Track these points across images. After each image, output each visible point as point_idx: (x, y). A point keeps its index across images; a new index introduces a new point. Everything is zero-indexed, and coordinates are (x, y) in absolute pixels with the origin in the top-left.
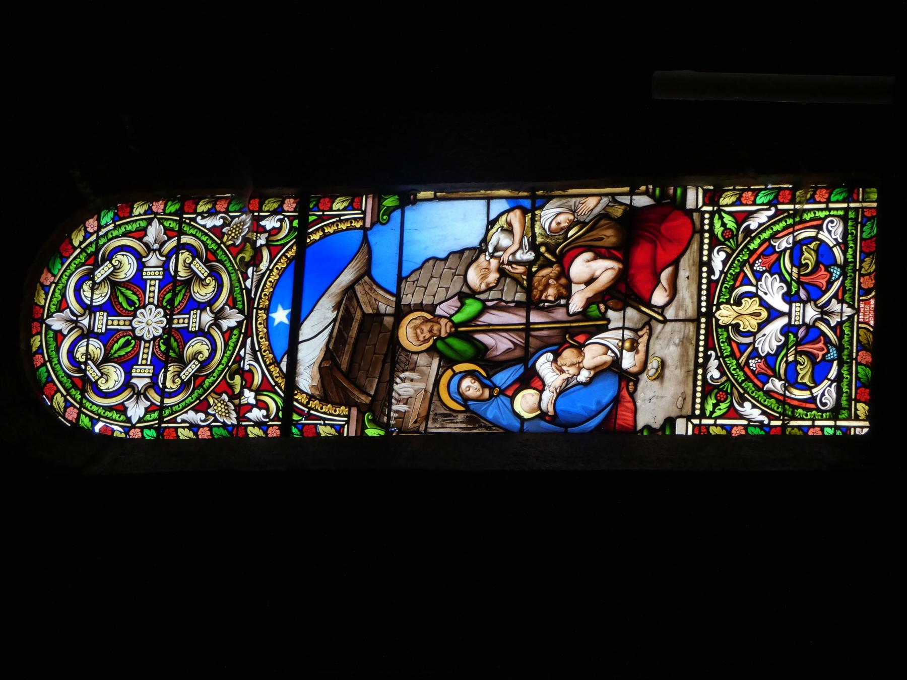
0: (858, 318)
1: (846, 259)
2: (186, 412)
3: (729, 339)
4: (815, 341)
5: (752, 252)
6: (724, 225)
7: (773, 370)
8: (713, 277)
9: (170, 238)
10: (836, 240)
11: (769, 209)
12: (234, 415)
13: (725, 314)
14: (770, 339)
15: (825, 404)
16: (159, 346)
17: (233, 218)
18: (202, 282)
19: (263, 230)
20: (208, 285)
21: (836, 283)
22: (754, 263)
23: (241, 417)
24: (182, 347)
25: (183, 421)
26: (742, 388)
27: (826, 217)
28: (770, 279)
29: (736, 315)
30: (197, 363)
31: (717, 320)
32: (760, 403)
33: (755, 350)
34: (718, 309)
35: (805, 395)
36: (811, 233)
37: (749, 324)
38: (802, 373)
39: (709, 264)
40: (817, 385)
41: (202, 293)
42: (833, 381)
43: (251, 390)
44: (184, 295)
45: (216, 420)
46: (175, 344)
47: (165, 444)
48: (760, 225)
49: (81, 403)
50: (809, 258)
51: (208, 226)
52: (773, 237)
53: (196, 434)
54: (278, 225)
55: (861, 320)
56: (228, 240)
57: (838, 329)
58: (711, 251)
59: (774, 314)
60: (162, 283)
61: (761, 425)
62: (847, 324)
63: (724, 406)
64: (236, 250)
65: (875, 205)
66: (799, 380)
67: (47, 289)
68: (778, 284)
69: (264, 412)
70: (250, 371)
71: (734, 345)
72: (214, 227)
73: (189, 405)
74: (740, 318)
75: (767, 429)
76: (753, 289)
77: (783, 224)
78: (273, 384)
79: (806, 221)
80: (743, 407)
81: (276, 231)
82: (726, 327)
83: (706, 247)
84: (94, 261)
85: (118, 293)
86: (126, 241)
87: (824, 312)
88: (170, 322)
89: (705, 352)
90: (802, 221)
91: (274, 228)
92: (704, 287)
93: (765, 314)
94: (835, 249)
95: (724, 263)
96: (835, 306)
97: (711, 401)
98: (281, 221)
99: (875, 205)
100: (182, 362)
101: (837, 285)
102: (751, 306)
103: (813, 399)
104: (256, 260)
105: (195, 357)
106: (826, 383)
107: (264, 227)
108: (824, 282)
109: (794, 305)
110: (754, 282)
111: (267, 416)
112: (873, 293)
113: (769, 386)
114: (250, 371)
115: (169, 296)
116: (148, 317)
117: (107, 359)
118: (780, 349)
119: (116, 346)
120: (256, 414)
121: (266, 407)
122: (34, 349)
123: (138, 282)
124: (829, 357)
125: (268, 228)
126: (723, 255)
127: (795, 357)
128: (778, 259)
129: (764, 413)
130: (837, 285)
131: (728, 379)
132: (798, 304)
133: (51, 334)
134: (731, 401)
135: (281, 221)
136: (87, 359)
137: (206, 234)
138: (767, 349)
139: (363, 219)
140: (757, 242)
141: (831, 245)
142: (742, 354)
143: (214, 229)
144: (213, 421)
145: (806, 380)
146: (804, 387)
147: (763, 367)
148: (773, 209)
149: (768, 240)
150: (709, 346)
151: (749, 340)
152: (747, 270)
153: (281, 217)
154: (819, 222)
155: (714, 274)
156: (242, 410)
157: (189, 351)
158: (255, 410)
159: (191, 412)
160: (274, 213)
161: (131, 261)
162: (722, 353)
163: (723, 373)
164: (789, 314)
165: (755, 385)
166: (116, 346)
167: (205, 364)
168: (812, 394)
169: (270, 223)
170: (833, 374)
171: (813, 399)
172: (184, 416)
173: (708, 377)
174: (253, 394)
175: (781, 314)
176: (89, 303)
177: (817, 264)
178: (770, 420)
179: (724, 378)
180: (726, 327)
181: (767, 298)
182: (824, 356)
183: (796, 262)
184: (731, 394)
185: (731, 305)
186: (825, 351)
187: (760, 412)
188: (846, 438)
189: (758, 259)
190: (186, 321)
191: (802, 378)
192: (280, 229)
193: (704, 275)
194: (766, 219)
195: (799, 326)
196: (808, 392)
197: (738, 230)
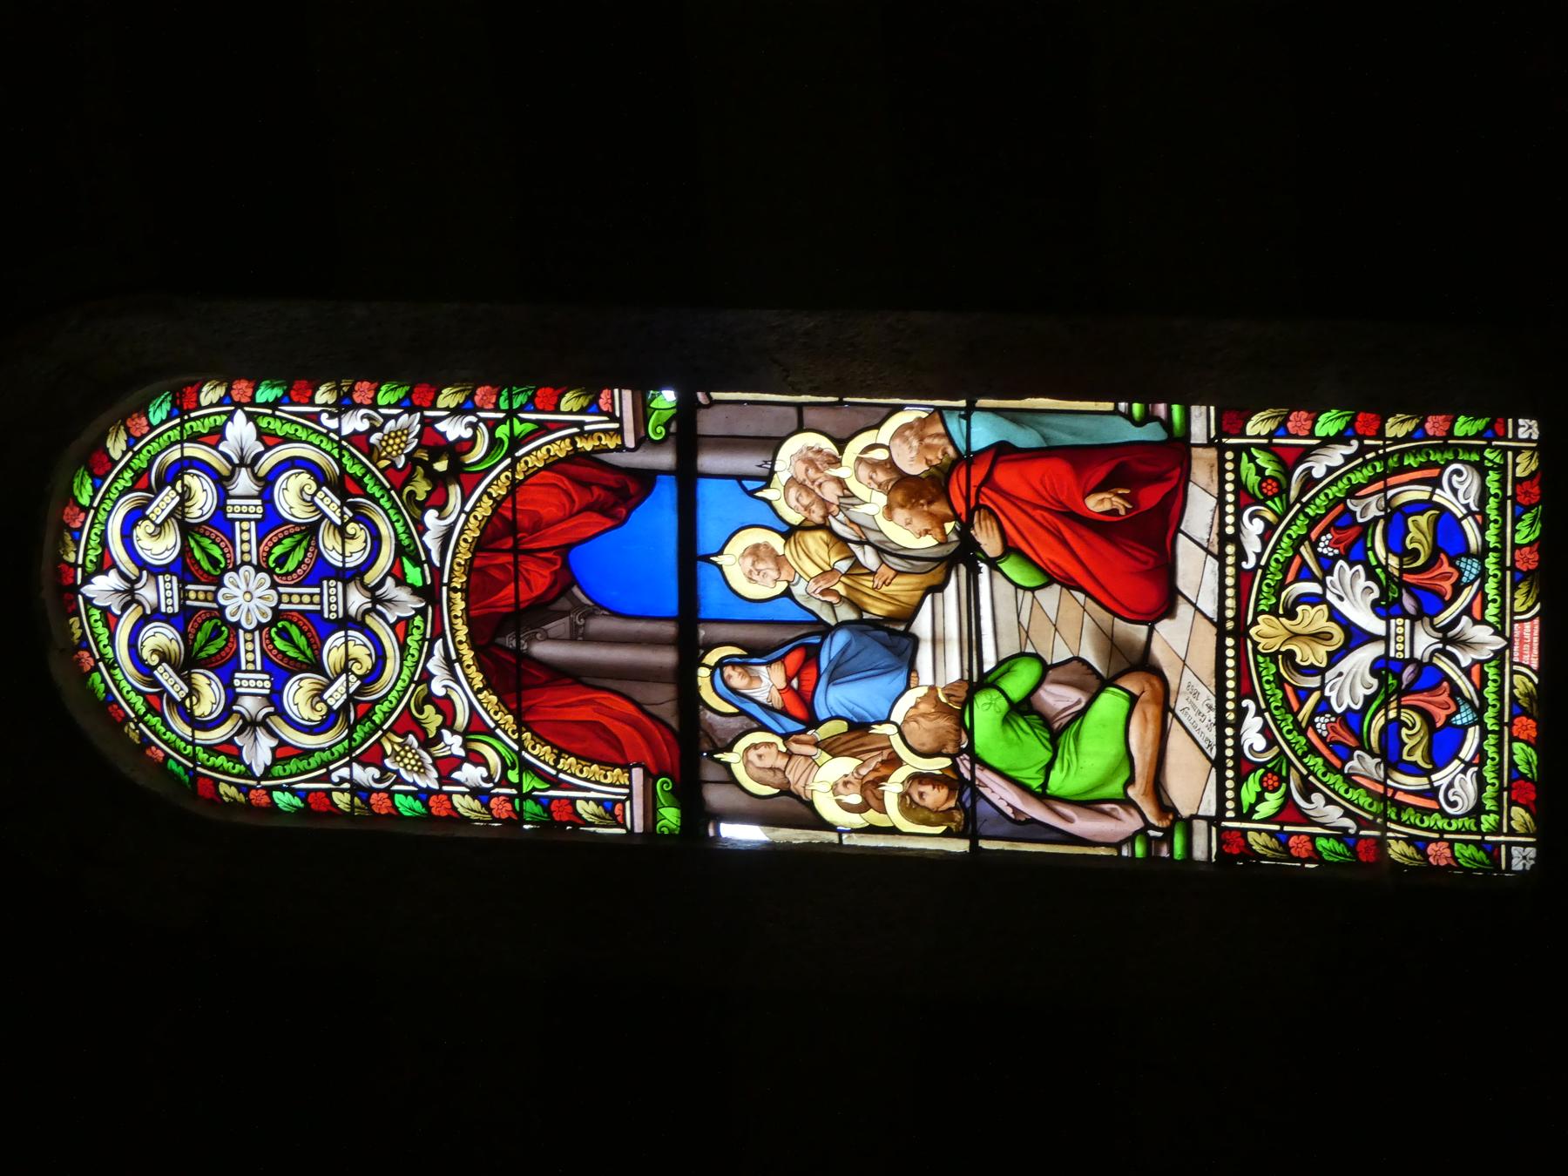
3: (1280, 681)
4: (1433, 688)
5: (1313, 522)
7: (1358, 735)
8: (1244, 565)
10: (1467, 506)
12: (434, 774)
13: (1267, 632)
14: (1352, 681)
15: (1453, 804)
17: (387, 418)
21: (1466, 591)
22: (1318, 540)
23: (444, 779)
26: (1305, 765)
28: (1349, 573)
31: (1255, 644)
33: (1324, 700)
35: (1419, 783)
36: (1419, 493)
37: (1316, 655)
38: (1410, 743)
39: (1236, 539)
40: (1436, 769)
42: (1468, 765)
43: (454, 732)
50: (1419, 532)
52: (1353, 492)
54: (468, 434)
55: (1516, 660)
58: (1238, 515)
59: (1356, 637)
61: (1342, 835)
66: (1405, 757)
68: (1362, 582)
69: (482, 771)
70: (447, 697)
71: (1289, 689)
72: (355, 433)
75: (1351, 841)
76: (1314, 588)
77: (1368, 472)
78: (492, 725)
80: (1309, 801)
82: (1273, 657)
83: (1230, 509)
86: (193, 450)
87: (1449, 638)
89: (1238, 701)
91: (460, 440)
93: (1339, 636)
94: (1464, 523)
98: (474, 426)
100: (185, 666)
101: (1467, 594)
102: (1314, 618)
103: (1432, 793)
108: (1447, 586)
109: (1393, 622)
111: (489, 779)
114: (447, 697)
118: (1369, 700)
120: (470, 774)
121: (480, 760)
124: (1459, 720)
126: (1258, 526)
127: (1399, 713)
129: (1348, 814)
134: (1288, 791)
138: (1347, 701)
139: (620, 432)
140: (1321, 501)
141: (1460, 515)
142: (1302, 704)
145: (1417, 757)
146: (1413, 770)
148: (1355, 443)
150: (1245, 690)
151: (1314, 682)
152: (1305, 551)
153: (472, 419)
154: (1434, 473)
155: (1246, 559)
158: (467, 767)
160: (457, 411)
162: (1268, 704)
164: (1386, 639)
166: (292, 653)
168: (1431, 782)
170: (1467, 751)
171: (1432, 793)
174: (458, 740)
175: (1371, 638)
178: (1360, 828)
179: (1276, 750)
181: (1345, 608)
182: (1449, 717)
183: (1395, 543)
184: (1287, 780)
185: (1278, 616)
187: (1340, 812)
190: (316, 599)
194: (1341, 461)
195: (1405, 663)
196: (1425, 780)
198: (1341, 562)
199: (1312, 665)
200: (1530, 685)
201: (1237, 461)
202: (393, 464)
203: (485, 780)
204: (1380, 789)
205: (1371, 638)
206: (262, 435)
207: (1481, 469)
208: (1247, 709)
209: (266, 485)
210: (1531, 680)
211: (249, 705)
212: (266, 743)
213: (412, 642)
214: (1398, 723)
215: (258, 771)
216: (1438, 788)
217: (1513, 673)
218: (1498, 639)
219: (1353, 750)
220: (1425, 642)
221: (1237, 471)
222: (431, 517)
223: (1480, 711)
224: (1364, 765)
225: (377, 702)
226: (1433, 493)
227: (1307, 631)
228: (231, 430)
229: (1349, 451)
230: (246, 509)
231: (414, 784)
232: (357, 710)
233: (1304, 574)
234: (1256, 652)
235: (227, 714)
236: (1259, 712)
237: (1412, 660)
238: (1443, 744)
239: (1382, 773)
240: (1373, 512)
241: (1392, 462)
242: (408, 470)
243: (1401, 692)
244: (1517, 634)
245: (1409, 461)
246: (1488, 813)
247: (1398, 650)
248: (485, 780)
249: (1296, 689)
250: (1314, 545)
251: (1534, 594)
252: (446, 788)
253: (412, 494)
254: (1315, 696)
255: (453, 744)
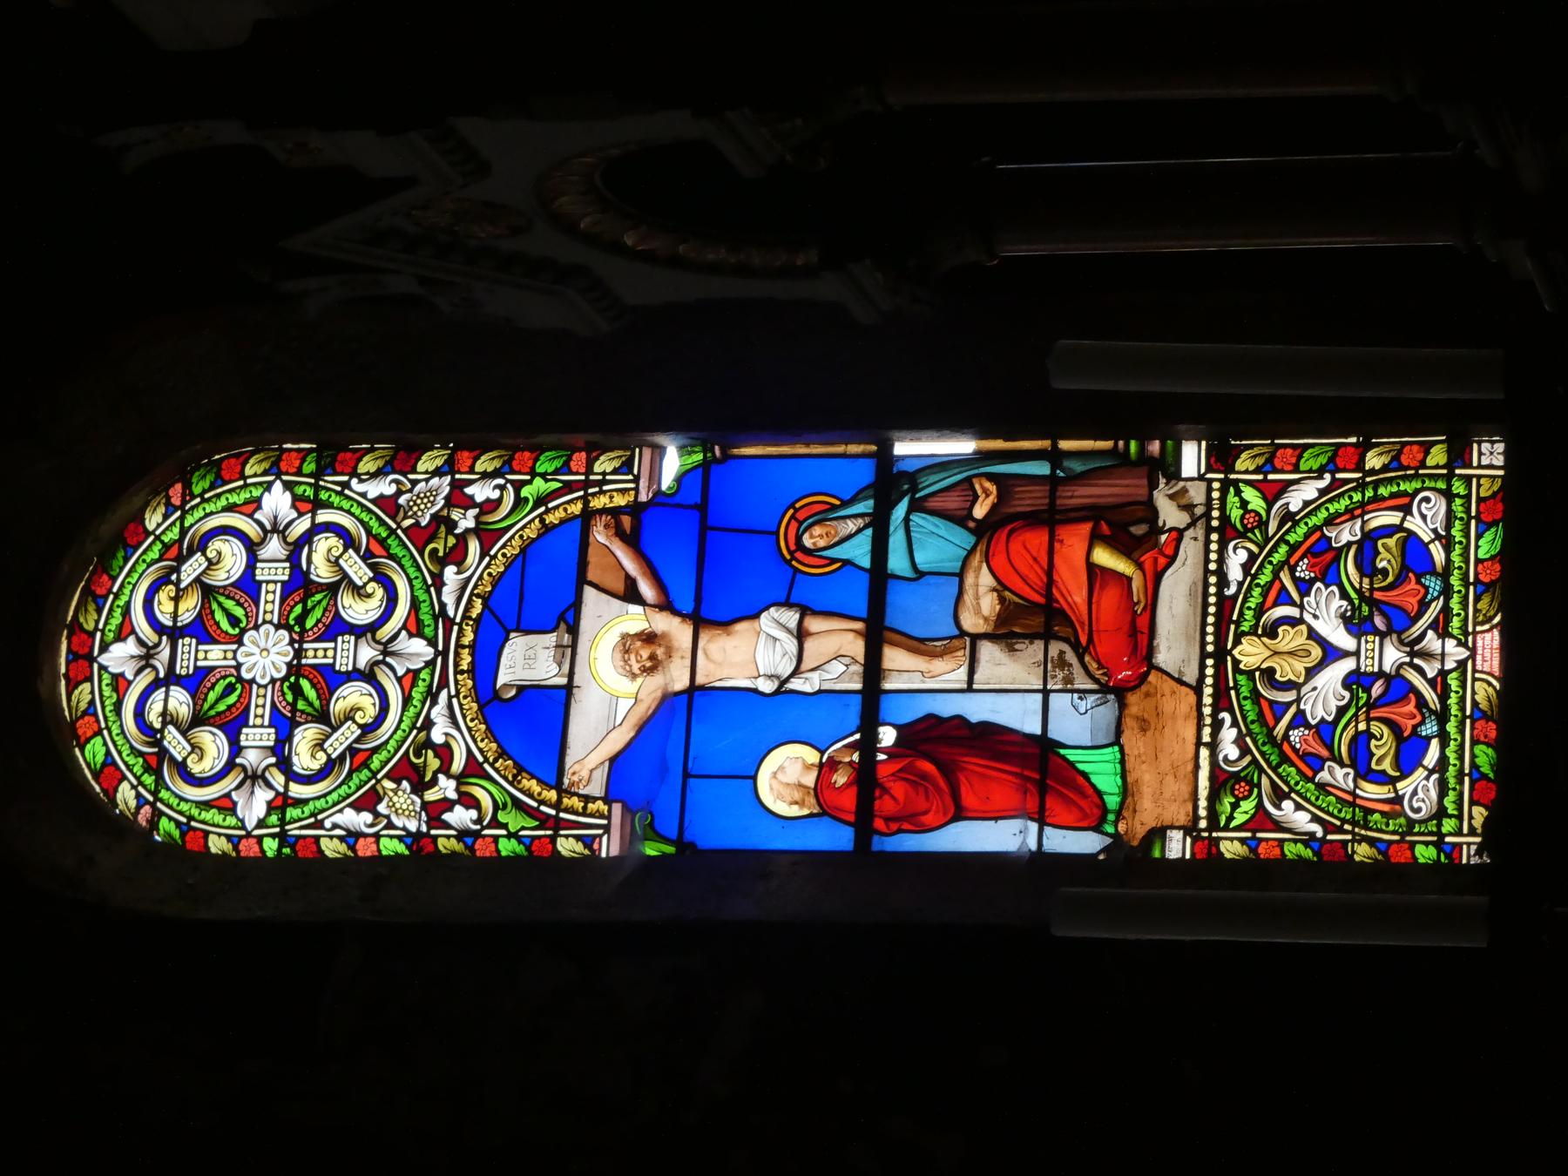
0: (1474, 665)
1: (1448, 560)
2: (341, 811)
3: (1256, 696)
4: (1402, 699)
5: (1293, 548)
6: (1244, 504)
7: (1330, 747)
9: (301, 514)
10: (1435, 531)
11: (1320, 477)
13: (1250, 653)
14: (1325, 694)
15: (1418, 810)
16: (283, 694)
18: (359, 592)
19: (469, 503)
20: (369, 596)
22: (1297, 564)
24: (325, 699)
25: (335, 826)
27: (1417, 491)
29: (1268, 653)
30: (354, 728)
31: (1236, 662)
32: (1308, 801)
33: (1300, 714)
34: (1237, 642)
36: (1392, 518)
37: (1288, 670)
38: (1378, 753)
40: (1403, 777)
41: (358, 611)
42: (1431, 772)
43: (449, 776)
44: (325, 610)
45: (390, 826)
46: (311, 693)
47: (301, 865)
48: (1306, 504)
49: (155, 793)
51: (370, 496)
52: (1330, 521)
53: (352, 848)
54: (496, 494)
56: (405, 517)
57: (1440, 683)
59: (1331, 654)
60: (288, 589)
61: (1308, 839)
62: (1454, 675)
63: (1248, 806)
64: (421, 536)
65: (1501, 473)
66: (1374, 766)
67: (101, 601)
69: (473, 814)
72: (382, 496)
73: (345, 799)
74: (1276, 658)
76: (1292, 611)
77: (1345, 502)
79: (1384, 499)
80: (1279, 808)
81: (491, 506)
82: (1250, 674)
84: (177, 554)
85: (215, 606)
87: (1414, 649)
88: (299, 654)
89: (1214, 715)
90: (1377, 499)
91: (488, 500)
92: (1212, 610)
93: (1317, 652)
94: (1431, 546)
95: (1246, 567)
96: (1432, 642)
97: (1228, 800)
98: (502, 488)
99: (1501, 473)
101: (1434, 609)
104: (457, 556)
105: (349, 716)
106: (1420, 773)
107: (471, 497)
108: (1414, 601)
110: (1295, 595)
111: (479, 821)
112: (1497, 619)
113: (1324, 776)
115: (298, 609)
116: (273, 657)
117: (198, 720)
118: (1341, 711)
119: (212, 696)
120: (460, 817)
122: (587, 852)
123: (248, 586)
125: (479, 499)
126: (1242, 556)
128: (1337, 560)
129: (1315, 819)
130: (1434, 609)
131: (1254, 761)
132: (1371, 638)
133: (106, 679)
135: (502, 488)
136: (164, 724)
137: (370, 511)
138: (1320, 713)
140: (1302, 530)
141: (1426, 539)
142: (1278, 720)
143: (380, 501)
144: (385, 828)
145: (1387, 766)
146: (1381, 778)
147: (1312, 742)
148: (1328, 476)
149: (1318, 528)
151: (1289, 696)
152: (1285, 577)
153: (502, 481)
154: (1405, 500)
156: (435, 812)
157: (338, 707)
158: (458, 808)
159: (349, 812)
161: (236, 551)
163: (1245, 751)
164: (1357, 654)
165: (1299, 771)
166: (212, 696)
167: (368, 729)
168: (1396, 791)
169: (481, 492)
170: (1432, 755)
172: (338, 818)
173: (1221, 757)
174: (452, 784)
175: (1345, 654)
176: (170, 624)
177: (1404, 569)
178: (1326, 832)
179: (1248, 758)
180: (1270, 664)
181: (1318, 626)
182: (1415, 727)
183: (1366, 565)
184: (1259, 785)
185: (1259, 637)
186: (1419, 718)
187: (1309, 816)
188: (1483, 865)
189: (1301, 559)
191: (1379, 762)
192: (499, 501)
193: (1212, 590)
194: (1316, 494)
197: (1268, 512)
198: (1318, 584)
199: (1290, 681)
200: (1490, 690)
201: (1224, 492)
202: (417, 524)
203: (475, 822)
204: (1350, 798)
205: (1345, 654)
206: (120, 637)
207: (1449, 495)
208: (1223, 720)
209: (296, 549)
210: (1490, 684)
211: (251, 758)
212: (263, 796)
213: (417, 695)
214: (1368, 735)
215: (250, 825)
216: (1403, 796)
217: (1474, 680)
218: (1461, 649)
219: (1324, 760)
220: (1393, 655)
221: (1223, 508)
222: (450, 571)
223: (1442, 717)
224: (1341, 776)
225: (375, 750)
226: (1403, 519)
227: (1286, 649)
228: (268, 502)
229: (1323, 484)
230: (273, 572)
231: (404, 829)
232: (357, 757)
233: (1283, 598)
234: (1236, 670)
235: (230, 766)
236: (1235, 724)
237: (1381, 674)
238: (1409, 754)
239: (1351, 785)
240: (1346, 537)
241: (1369, 493)
242: (432, 529)
243: (1370, 706)
244: (1479, 643)
245: (1383, 491)
246: (1450, 816)
247: (1369, 666)
248: (475, 822)
249: (1271, 703)
250: (1292, 570)
251: (1496, 604)
252: (433, 832)
253: (435, 551)
254: (1293, 710)
255: (447, 788)
